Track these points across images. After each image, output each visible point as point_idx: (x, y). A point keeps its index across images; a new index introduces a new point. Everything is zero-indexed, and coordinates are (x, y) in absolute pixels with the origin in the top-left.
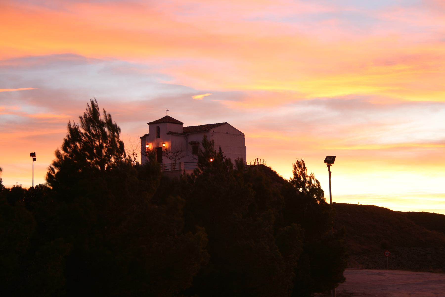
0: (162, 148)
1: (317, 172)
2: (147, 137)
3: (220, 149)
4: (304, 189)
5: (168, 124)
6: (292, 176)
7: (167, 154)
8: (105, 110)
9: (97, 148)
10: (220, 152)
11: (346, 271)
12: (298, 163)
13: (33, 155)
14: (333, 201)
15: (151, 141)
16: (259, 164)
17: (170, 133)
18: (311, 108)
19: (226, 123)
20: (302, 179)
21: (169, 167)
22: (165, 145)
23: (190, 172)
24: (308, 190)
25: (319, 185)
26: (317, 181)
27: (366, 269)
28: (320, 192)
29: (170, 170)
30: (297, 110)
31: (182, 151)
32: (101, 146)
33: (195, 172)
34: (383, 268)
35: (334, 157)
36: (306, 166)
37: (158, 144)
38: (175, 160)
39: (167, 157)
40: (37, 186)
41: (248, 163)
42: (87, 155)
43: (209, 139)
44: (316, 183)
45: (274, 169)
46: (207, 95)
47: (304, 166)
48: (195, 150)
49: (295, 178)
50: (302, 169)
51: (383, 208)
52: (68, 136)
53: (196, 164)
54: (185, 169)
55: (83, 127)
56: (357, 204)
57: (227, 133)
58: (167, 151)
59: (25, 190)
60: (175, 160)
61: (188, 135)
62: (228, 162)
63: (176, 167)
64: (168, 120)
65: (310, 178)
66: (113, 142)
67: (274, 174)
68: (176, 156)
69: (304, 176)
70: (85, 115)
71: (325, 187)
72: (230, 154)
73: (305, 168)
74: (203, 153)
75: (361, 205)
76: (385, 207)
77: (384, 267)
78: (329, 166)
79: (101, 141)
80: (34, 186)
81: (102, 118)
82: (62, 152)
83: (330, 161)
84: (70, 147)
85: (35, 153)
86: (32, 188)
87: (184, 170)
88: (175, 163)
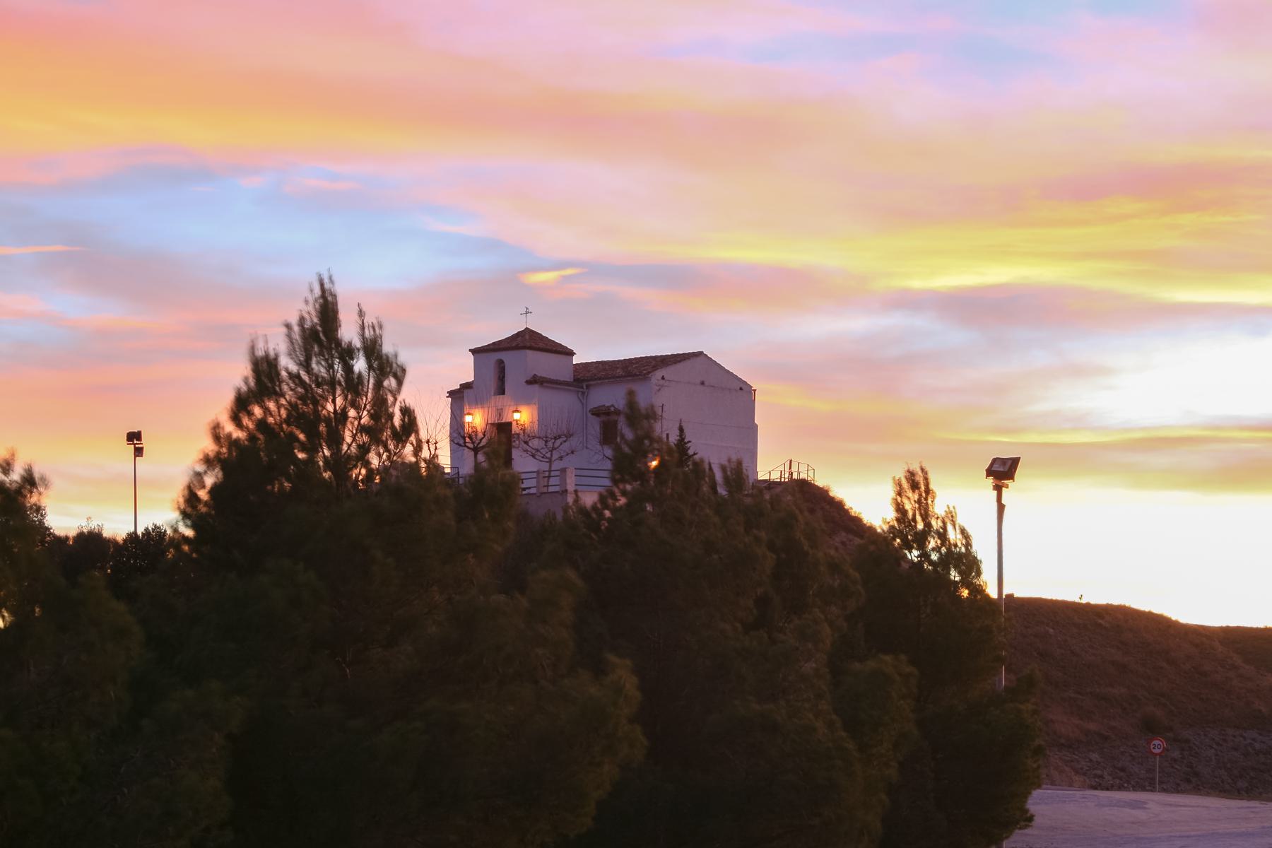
0: (510, 424)
1: (963, 503)
2: (466, 391)
3: (681, 430)
4: (925, 555)
5: (529, 352)
6: (891, 515)
7: (526, 443)
8: (364, 309)
9: (327, 420)
10: (682, 444)
11: (1036, 793)
12: (911, 476)
13: (134, 437)
14: (1006, 592)
15: (479, 402)
16: (795, 476)
17: (534, 381)
18: (895, 321)
19: (701, 353)
20: (920, 526)
21: (533, 483)
22: (522, 417)
23: (589, 499)
24: (934, 557)
25: (968, 545)
26: (963, 531)
27: (1095, 788)
28: (969, 564)
29: (533, 491)
30: (855, 325)
31: (569, 436)
32: (342, 417)
33: (602, 499)
34: (1144, 789)
35: (1015, 462)
36: (931, 486)
37: (500, 413)
38: (550, 461)
39: (526, 451)
40: (147, 529)
41: (762, 475)
42: (297, 440)
43: (642, 401)
44: (959, 536)
45: (837, 492)
46: (569, 272)
47: (927, 485)
48: (608, 435)
49: (898, 520)
50: (920, 495)
51: (1150, 613)
52: (246, 380)
53: (606, 474)
54: (579, 488)
55: (291, 354)
56: (1077, 600)
57: (703, 383)
58: (526, 436)
59: (113, 542)
60: (550, 461)
61: (588, 387)
62: (700, 471)
63: (553, 481)
64: (528, 341)
65: (944, 522)
66: (380, 409)
67: (837, 507)
68: (554, 449)
69: (926, 517)
70: (302, 320)
71: (984, 551)
72: (709, 449)
73: (928, 491)
74: (626, 442)
75: (1088, 605)
76: (1156, 611)
77: (1146, 784)
78: (998, 488)
79: (339, 401)
80: (140, 532)
81: (349, 332)
82: (229, 427)
83: (1002, 471)
84: (250, 414)
85: (139, 433)
86: (132, 537)
87: (576, 491)
88: (550, 471)
